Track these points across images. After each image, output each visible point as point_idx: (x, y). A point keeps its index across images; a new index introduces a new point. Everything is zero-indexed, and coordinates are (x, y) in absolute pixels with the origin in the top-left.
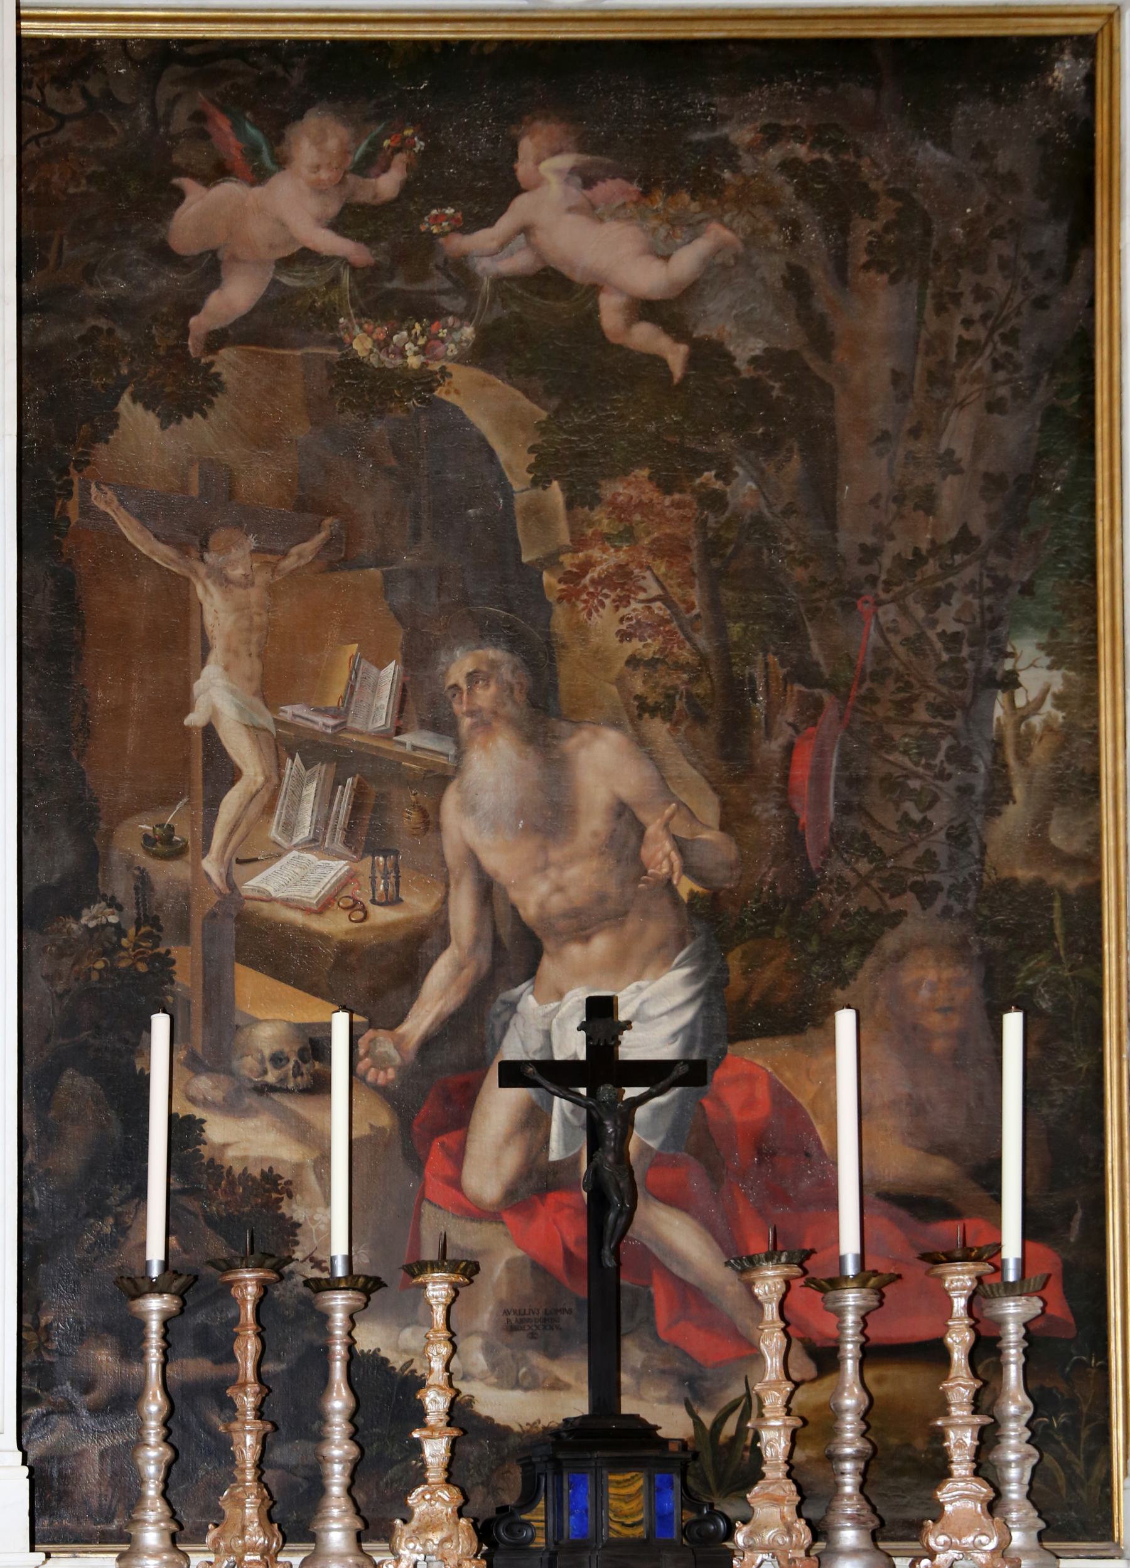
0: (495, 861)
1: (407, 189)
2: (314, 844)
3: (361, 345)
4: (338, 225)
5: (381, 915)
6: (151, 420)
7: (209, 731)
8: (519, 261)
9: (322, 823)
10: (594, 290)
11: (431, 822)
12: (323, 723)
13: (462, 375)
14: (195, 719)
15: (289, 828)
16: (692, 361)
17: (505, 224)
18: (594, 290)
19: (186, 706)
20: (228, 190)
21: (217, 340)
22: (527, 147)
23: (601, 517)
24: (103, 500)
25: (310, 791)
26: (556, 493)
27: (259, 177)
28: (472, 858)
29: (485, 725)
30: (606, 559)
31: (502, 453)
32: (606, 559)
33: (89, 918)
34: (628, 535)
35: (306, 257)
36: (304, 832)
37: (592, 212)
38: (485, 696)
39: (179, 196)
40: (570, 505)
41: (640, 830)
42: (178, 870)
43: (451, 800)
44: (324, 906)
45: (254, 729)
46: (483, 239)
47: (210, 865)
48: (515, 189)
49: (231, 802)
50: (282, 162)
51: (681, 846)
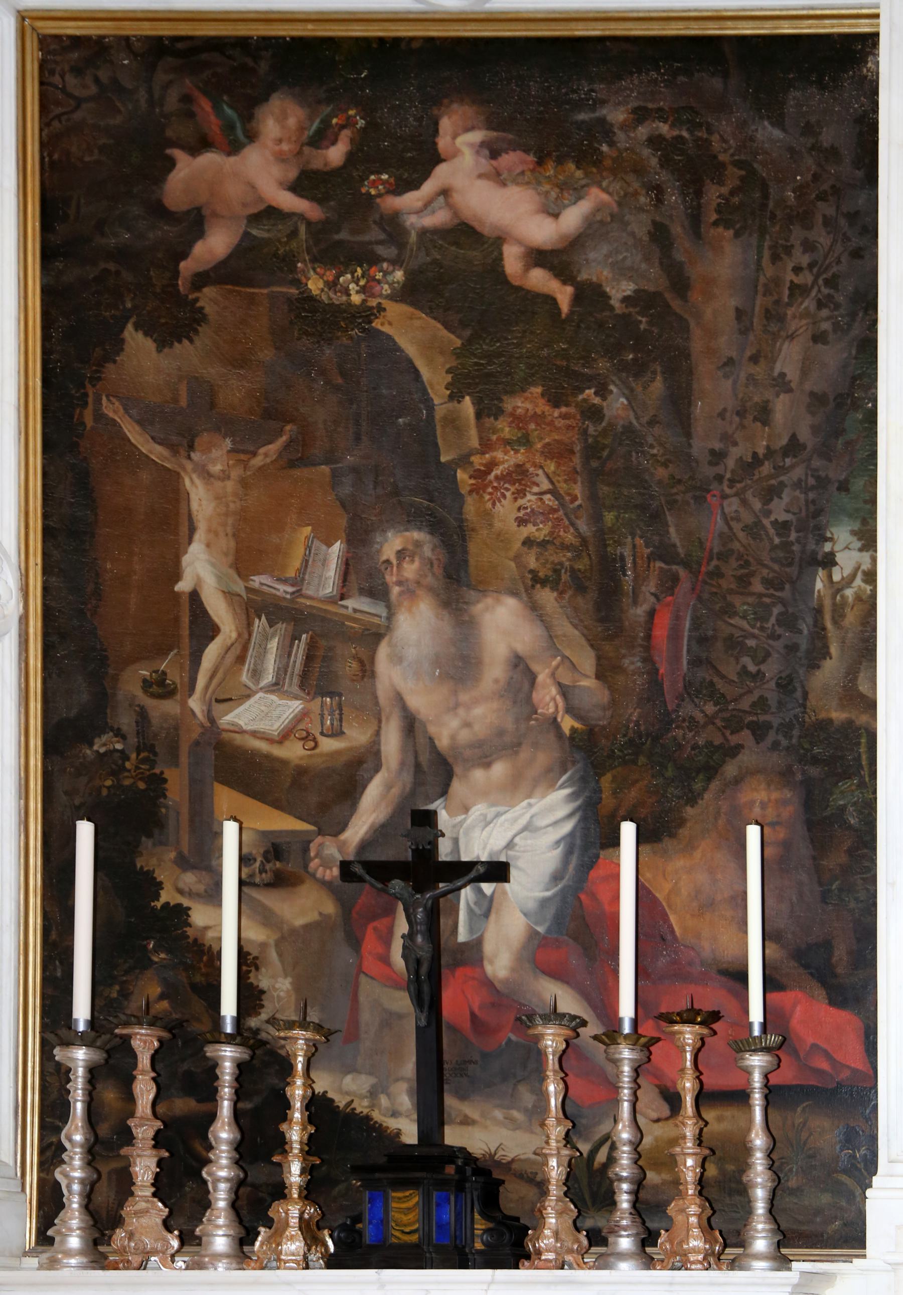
0: (417, 702)
1: (351, 158)
2: (276, 687)
3: (315, 285)
4: (296, 188)
5: (328, 745)
6: (149, 344)
7: (195, 596)
8: (439, 218)
9: (282, 672)
10: (499, 241)
11: (367, 670)
12: (284, 590)
13: (394, 310)
14: (183, 586)
15: (256, 674)
16: (577, 299)
17: (429, 187)
18: (499, 241)
19: (177, 576)
20: (209, 159)
21: (201, 280)
22: (446, 124)
23: (504, 428)
24: (112, 409)
25: (273, 645)
26: (468, 406)
27: (234, 148)
28: (399, 699)
29: (410, 593)
30: (507, 459)
31: (425, 373)
32: (507, 459)
33: (101, 744)
34: (525, 441)
35: (271, 213)
36: (269, 678)
37: (498, 178)
38: (411, 570)
39: (171, 164)
40: (479, 415)
41: (532, 678)
42: (170, 707)
43: (383, 651)
44: (285, 736)
45: (229, 595)
46: (411, 199)
47: (195, 704)
48: (436, 159)
49: (211, 653)
50: (252, 137)
51: (564, 691)
